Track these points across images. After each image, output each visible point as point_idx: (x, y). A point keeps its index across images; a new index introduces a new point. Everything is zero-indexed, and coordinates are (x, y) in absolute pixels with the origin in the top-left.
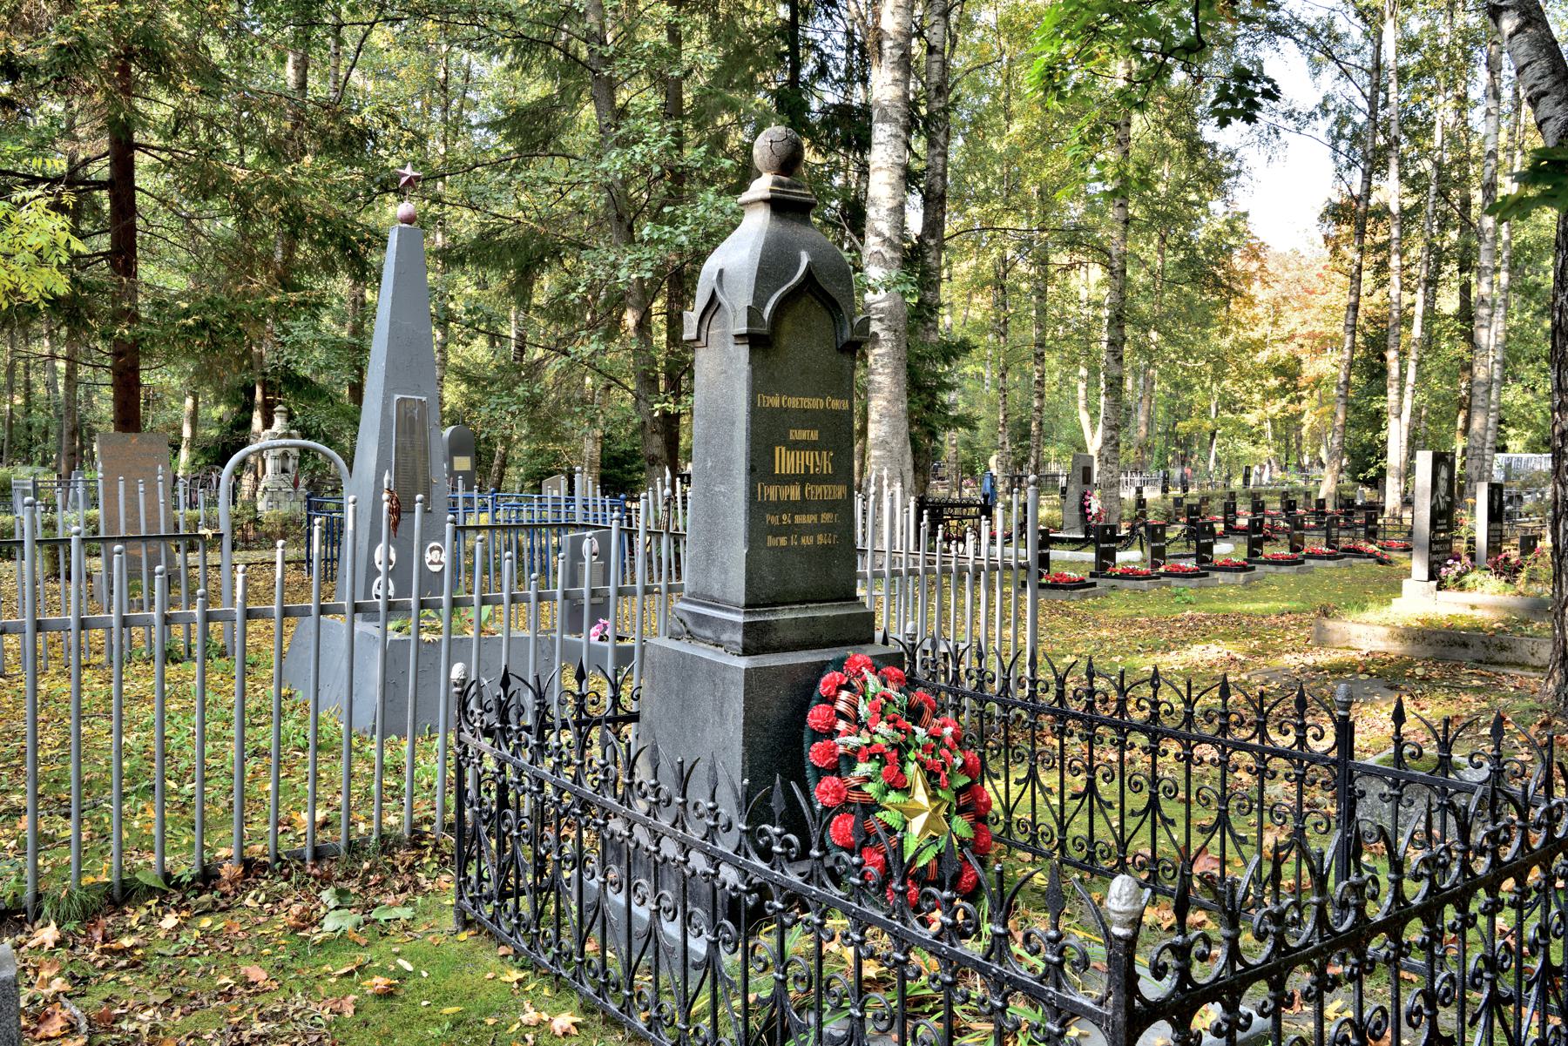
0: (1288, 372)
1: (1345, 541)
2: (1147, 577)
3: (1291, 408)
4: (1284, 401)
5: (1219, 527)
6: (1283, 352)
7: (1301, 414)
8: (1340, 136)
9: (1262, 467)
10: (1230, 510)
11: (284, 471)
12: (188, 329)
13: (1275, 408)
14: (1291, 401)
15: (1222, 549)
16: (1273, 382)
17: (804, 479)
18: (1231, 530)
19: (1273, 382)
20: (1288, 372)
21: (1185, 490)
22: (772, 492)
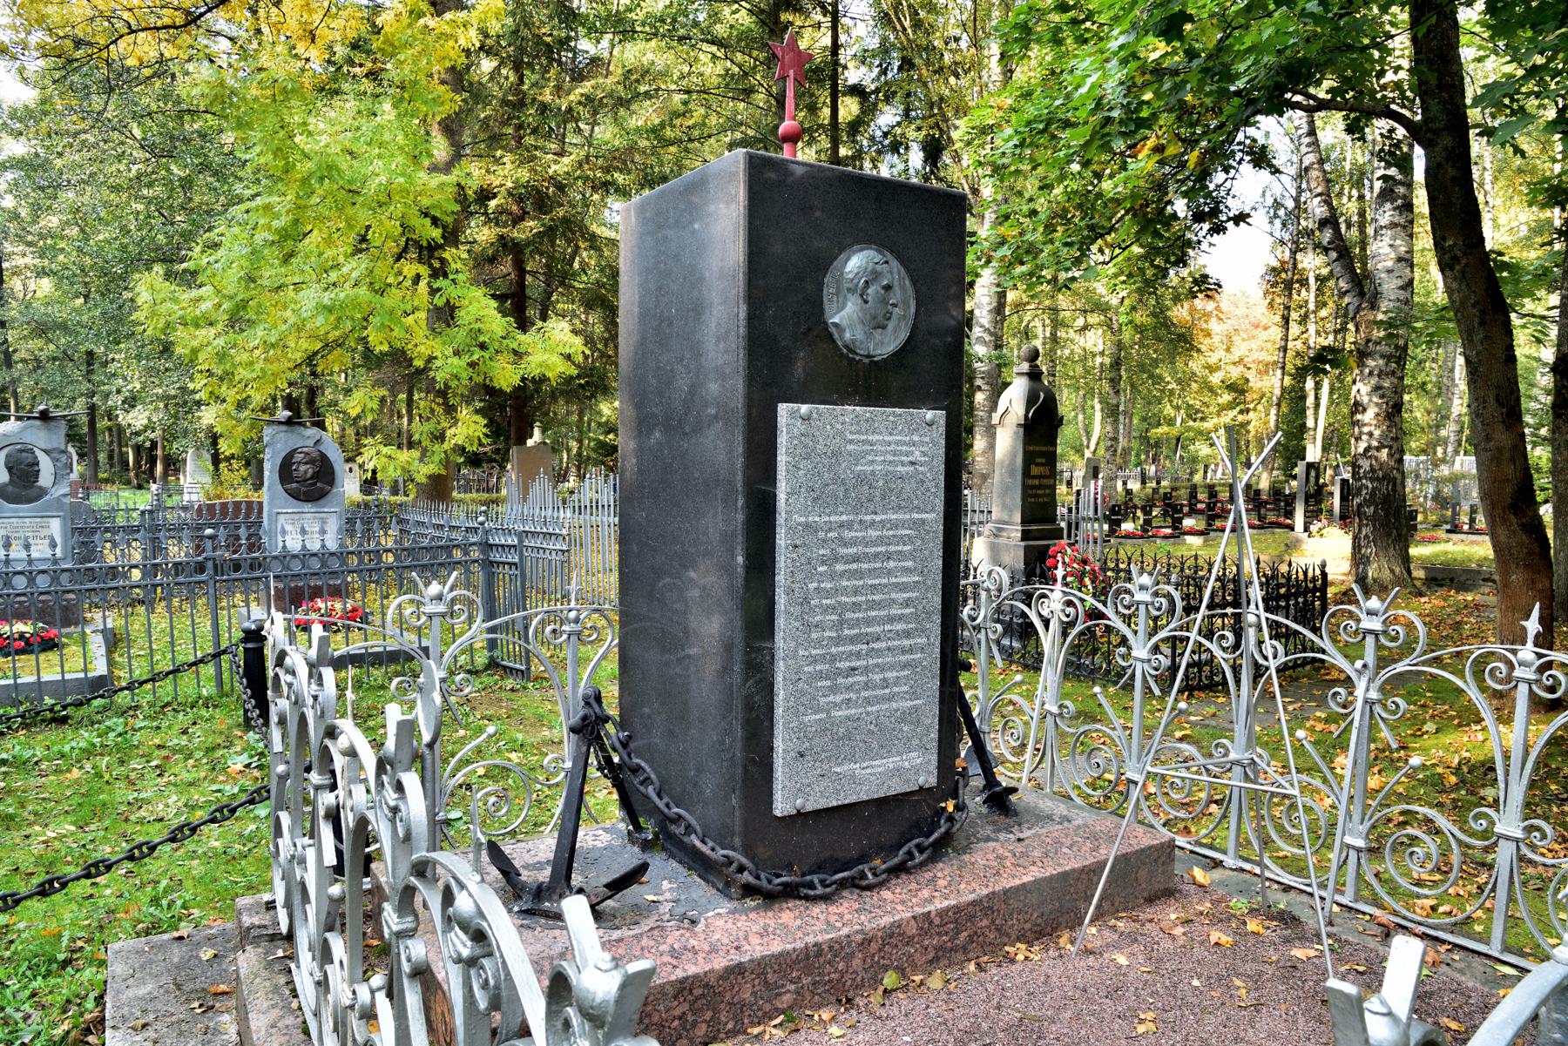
0: (1238, 389)
1: (1271, 517)
2: (1142, 537)
3: (1240, 418)
4: (1235, 412)
5: (1186, 509)
6: (1235, 373)
7: (1249, 423)
8: (1276, 216)
9: (1217, 465)
10: (1193, 495)
12: (581, 386)
13: (1228, 417)
14: (1241, 412)
15: (1188, 523)
16: (1226, 397)
17: (1040, 477)
18: (1193, 511)
19: (1226, 397)
20: (1238, 389)
21: (1158, 483)
22: (1030, 482)
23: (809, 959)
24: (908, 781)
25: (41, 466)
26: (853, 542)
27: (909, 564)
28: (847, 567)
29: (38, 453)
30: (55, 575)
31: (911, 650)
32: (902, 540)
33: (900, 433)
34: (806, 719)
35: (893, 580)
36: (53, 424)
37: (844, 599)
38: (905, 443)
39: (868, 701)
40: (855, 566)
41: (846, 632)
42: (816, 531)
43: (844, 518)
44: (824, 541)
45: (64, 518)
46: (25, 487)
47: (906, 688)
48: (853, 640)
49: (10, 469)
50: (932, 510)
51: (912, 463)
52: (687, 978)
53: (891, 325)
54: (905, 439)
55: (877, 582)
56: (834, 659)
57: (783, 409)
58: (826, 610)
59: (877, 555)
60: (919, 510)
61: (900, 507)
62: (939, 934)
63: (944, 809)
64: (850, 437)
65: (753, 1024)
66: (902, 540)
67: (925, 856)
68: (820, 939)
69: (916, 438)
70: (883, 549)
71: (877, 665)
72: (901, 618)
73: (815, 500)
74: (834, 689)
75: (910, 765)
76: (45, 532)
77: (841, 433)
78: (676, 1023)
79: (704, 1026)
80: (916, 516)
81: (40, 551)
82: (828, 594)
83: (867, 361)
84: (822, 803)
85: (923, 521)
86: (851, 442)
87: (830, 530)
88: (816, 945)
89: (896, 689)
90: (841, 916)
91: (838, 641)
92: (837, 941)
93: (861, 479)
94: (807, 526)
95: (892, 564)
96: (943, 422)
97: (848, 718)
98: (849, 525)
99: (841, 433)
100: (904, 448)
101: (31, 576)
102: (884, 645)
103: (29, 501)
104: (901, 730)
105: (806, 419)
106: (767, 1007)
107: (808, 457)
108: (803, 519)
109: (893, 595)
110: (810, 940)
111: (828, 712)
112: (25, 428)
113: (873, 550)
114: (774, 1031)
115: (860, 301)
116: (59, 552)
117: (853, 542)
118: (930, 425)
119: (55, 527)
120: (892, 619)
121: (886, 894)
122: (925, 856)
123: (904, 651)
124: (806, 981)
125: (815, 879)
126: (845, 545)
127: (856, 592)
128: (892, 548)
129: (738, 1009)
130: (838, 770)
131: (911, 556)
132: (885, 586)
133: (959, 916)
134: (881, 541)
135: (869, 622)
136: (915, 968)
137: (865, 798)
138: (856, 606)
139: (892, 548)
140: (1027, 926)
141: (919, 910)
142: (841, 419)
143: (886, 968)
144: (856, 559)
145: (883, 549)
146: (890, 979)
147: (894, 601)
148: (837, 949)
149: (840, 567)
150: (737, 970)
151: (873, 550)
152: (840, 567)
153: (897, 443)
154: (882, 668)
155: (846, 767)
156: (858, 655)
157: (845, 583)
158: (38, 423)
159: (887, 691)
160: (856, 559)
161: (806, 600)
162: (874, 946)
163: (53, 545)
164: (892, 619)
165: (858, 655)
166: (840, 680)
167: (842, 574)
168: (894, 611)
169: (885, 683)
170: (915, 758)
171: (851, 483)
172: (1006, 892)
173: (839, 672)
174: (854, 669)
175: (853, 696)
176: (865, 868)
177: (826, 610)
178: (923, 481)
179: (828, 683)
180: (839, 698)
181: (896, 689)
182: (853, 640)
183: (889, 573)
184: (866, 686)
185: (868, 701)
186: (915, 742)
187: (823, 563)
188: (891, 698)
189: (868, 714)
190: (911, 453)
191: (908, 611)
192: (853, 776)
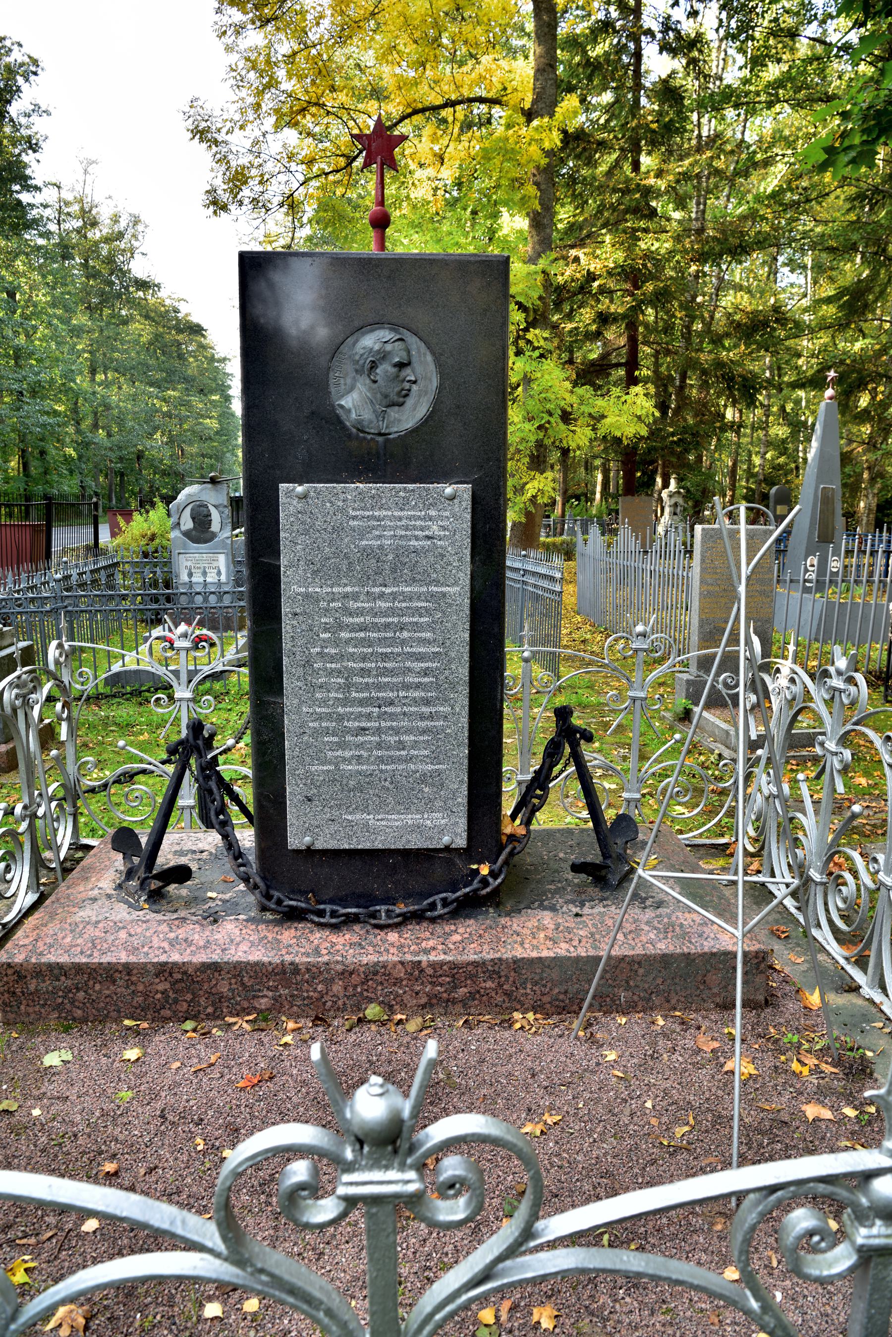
11: (675, 514)
23: (285, 973)
24: (431, 838)
25: (213, 517)
26: (360, 612)
27: (428, 635)
28: (353, 635)
29: (211, 508)
30: (220, 595)
31: (431, 717)
32: (418, 612)
33: (413, 508)
34: (313, 768)
35: (408, 649)
36: (219, 486)
37: (350, 664)
38: (419, 518)
39: (381, 760)
40: (362, 635)
41: (354, 694)
42: (318, 601)
43: (349, 589)
44: (327, 610)
45: (227, 554)
46: (203, 532)
47: (426, 752)
48: (361, 702)
49: (193, 519)
50: (456, 584)
51: (428, 538)
52: (167, 963)
53: (410, 402)
54: (441, 513)
55: (389, 650)
56: (341, 718)
57: (283, 486)
58: (331, 673)
59: (387, 626)
60: (437, 583)
61: (414, 580)
62: (433, 984)
63: (477, 871)
64: (352, 513)
65: (232, 1016)
66: (418, 612)
67: (446, 910)
68: (297, 960)
69: (433, 513)
70: (396, 620)
71: (391, 728)
72: (418, 686)
73: (315, 573)
74: (342, 745)
75: (444, 825)
76: (215, 564)
77: (343, 511)
78: (159, 996)
79: (185, 1005)
80: (435, 589)
81: (211, 578)
82: (332, 659)
83: (380, 439)
84: (332, 845)
85: (444, 595)
86: (354, 518)
87: (333, 600)
88: (292, 964)
89: (413, 752)
90: (333, 945)
91: (345, 702)
92: (316, 965)
93: (367, 553)
94: (307, 596)
95: (406, 634)
96: (467, 503)
97: (359, 773)
98: (355, 597)
99: (343, 511)
100: (418, 523)
101: (206, 596)
102: (399, 710)
103: (206, 542)
104: (421, 791)
105: (304, 496)
106: (245, 1004)
107: (306, 533)
108: (303, 590)
109: (408, 664)
110: (288, 958)
111: (337, 765)
112: (202, 490)
113: (383, 620)
114: (245, 1025)
115: (368, 381)
116: (223, 578)
117: (360, 612)
118: (452, 498)
119: (222, 561)
120: (407, 687)
121: (393, 936)
122: (446, 910)
123: (422, 717)
124: (284, 992)
125: (328, 908)
126: (351, 615)
127: (364, 658)
128: (406, 619)
129: (218, 1000)
130: (349, 817)
131: (430, 627)
132: (399, 655)
133: (456, 973)
134: (391, 612)
135: (380, 687)
136: (404, 1007)
137: (380, 846)
138: (364, 672)
139: (406, 619)
140: (546, 999)
141: (409, 957)
142: (342, 496)
143: (370, 1000)
144: (363, 628)
145: (396, 620)
146: (372, 1011)
147: (409, 670)
148: (314, 972)
149: (344, 635)
150: (214, 967)
151: (383, 620)
152: (344, 635)
153: (410, 518)
154: (397, 731)
155: (358, 816)
156: (369, 717)
157: (351, 650)
158: (209, 486)
159: (403, 753)
160: (363, 628)
161: (308, 663)
162: (355, 979)
163: (219, 573)
164: (407, 687)
165: (369, 717)
166: (349, 738)
167: (348, 641)
168: (409, 679)
169: (401, 745)
170: (439, 819)
171: (355, 557)
172: (516, 961)
173: (348, 731)
174: (364, 729)
175: (365, 754)
176: (383, 908)
177: (331, 673)
178: (442, 556)
179: (336, 739)
180: (348, 754)
181: (413, 752)
182: (361, 702)
183: (403, 642)
184: (379, 746)
185: (381, 760)
186: (438, 804)
187: (326, 630)
188: (409, 759)
189: (381, 771)
190: (428, 528)
191: (426, 680)
192: (366, 825)
